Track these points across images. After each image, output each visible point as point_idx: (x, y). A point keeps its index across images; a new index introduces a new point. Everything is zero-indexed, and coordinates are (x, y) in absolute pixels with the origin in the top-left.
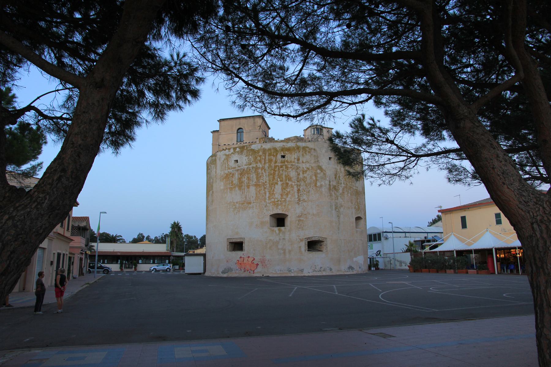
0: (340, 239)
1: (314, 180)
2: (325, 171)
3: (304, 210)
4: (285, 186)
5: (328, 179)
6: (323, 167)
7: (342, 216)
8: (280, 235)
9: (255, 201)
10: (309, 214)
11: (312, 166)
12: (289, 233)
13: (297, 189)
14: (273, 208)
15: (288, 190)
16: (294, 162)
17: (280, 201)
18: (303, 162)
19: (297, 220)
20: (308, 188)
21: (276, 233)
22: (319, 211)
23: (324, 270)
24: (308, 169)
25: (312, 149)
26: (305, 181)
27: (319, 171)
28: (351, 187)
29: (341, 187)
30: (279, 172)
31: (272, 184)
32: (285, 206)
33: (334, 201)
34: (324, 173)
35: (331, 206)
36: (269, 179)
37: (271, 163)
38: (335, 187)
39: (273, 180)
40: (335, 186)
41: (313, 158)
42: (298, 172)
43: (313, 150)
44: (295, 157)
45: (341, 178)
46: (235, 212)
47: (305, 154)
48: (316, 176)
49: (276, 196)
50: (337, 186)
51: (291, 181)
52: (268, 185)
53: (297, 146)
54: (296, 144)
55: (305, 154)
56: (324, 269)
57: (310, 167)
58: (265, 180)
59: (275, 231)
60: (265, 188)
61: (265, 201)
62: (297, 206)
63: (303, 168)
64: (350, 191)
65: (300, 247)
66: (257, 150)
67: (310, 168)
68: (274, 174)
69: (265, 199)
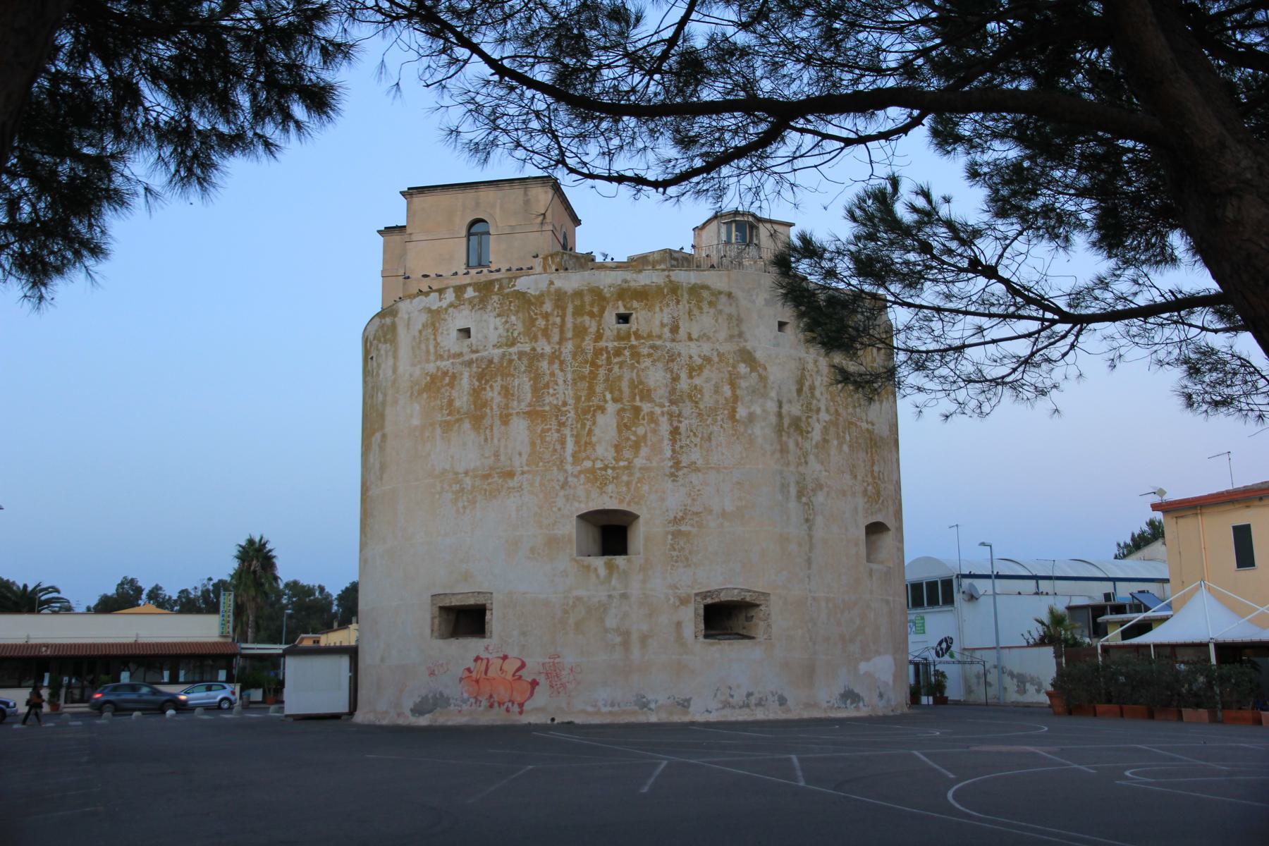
0: (814, 598)
2: (765, 369)
3: (693, 500)
5: (773, 394)
6: (759, 355)
9: (526, 468)
10: (711, 511)
15: (641, 431)
16: (660, 337)
17: (614, 469)
18: (690, 339)
19: (668, 533)
21: (598, 576)
24: (708, 360)
25: (720, 293)
26: (697, 403)
27: (743, 368)
29: (818, 420)
30: (610, 370)
31: (585, 412)
32: (628, 484)
33: (792, 468)
34: (760, 376)
36: (575, 394)
37: (583, 340)
39: (589, 399)
40: (798, 419)
43: (723, 299)
44: (665, 321)
45: (817, 393)
47: (696, 311)
48: (733, 385)
49: (600, 450)
50: (804, 419)
51: (651, 400)
52: (572, 414)
53: (670, 281)
55: (696, 311)
56: (761, 699)
57: (715, 354)
58: (561, 397)
59: (596, 569)
60: (562, 424)
63: (691, 357)
66: (534, 297)
68: (593, 375)
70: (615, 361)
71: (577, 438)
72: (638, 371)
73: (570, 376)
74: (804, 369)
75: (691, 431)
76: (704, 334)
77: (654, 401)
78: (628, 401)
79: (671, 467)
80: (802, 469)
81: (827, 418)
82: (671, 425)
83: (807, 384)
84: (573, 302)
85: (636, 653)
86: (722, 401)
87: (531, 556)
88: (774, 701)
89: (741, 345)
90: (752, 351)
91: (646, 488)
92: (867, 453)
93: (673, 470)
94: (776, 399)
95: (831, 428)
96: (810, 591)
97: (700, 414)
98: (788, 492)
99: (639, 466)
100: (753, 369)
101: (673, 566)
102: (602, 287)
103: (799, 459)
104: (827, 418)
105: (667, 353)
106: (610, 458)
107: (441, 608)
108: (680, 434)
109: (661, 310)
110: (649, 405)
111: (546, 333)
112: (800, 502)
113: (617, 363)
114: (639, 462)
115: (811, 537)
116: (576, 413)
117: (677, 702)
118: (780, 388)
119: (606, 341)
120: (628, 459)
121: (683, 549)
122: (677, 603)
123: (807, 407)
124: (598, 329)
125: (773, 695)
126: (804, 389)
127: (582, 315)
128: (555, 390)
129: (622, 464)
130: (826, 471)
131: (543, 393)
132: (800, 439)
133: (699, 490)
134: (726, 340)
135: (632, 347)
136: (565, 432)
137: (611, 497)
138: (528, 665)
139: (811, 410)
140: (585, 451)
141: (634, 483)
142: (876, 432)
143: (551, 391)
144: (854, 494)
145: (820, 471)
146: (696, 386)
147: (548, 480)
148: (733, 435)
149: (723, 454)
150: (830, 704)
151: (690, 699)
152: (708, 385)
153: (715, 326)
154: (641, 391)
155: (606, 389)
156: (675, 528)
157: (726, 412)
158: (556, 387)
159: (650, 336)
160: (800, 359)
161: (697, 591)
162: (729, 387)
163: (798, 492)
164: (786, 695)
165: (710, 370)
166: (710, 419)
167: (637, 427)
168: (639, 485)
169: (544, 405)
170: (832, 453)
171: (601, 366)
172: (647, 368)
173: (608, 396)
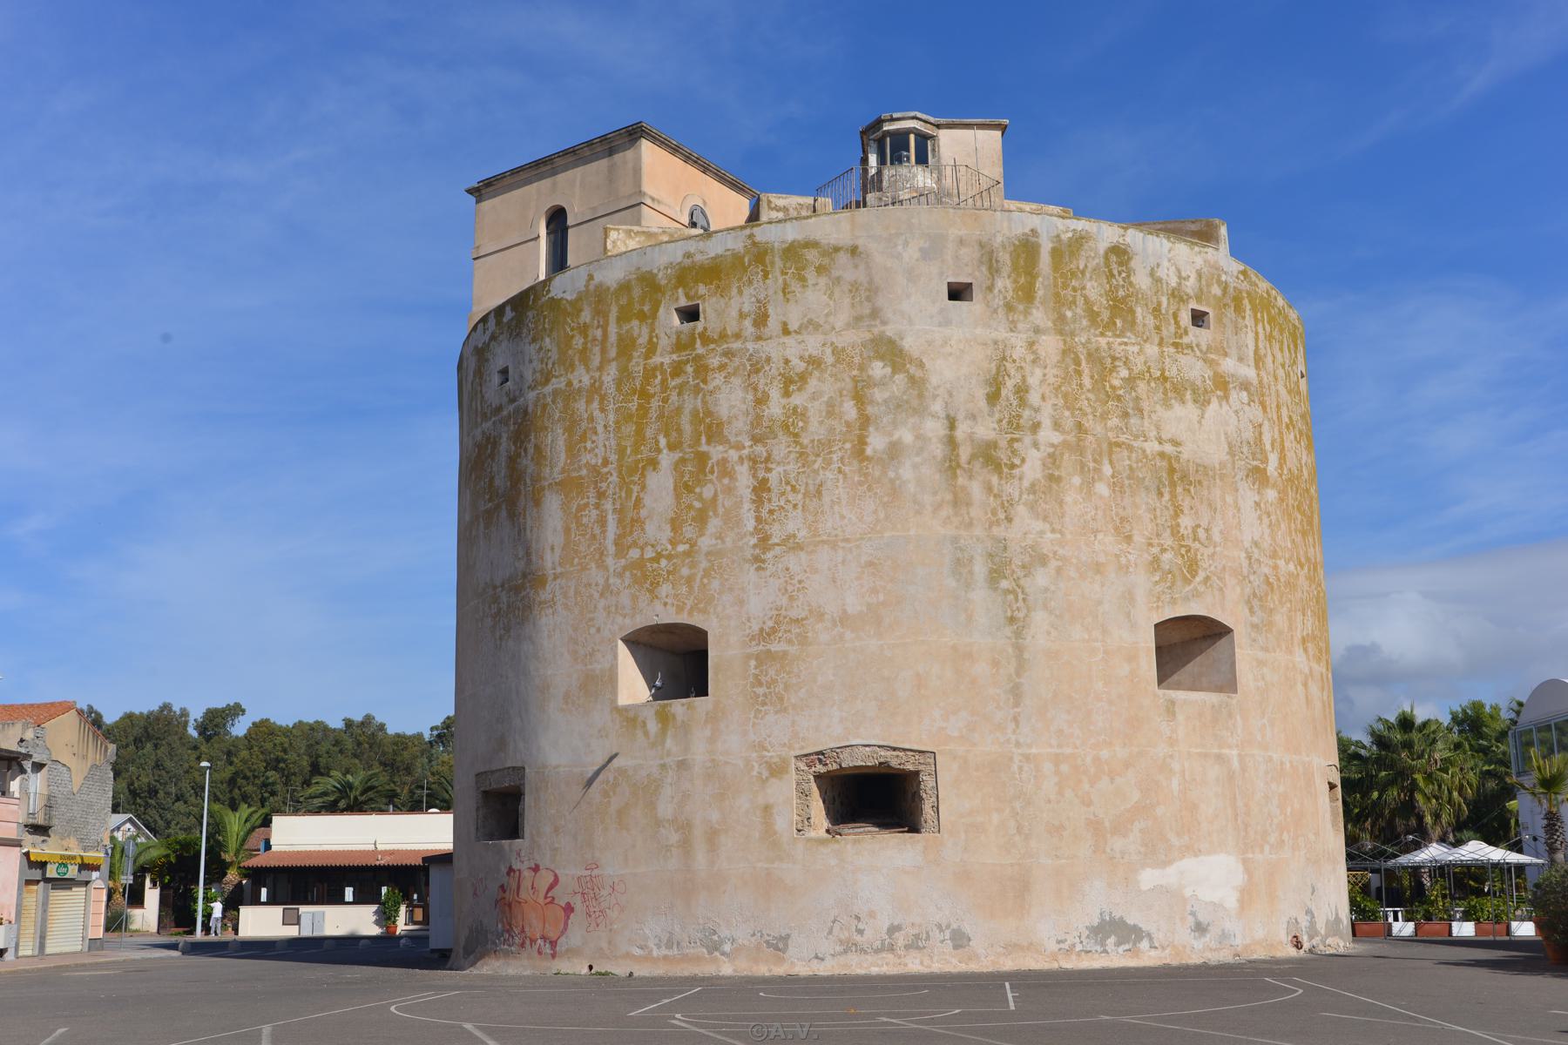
0: (1027, 758)
1: (848, 424)
2: (921, 365)
3: (791, 598)
4: (695, 470)
5: (937, 407)
6: (909, 344)
7: (1039, 618)
8: (663, 743)
9: (559, 570)
10: (821, 616)
11: (840, 342)
12: (708, 733)
13: (751, 482)
14: (634, 598)
15: (708, 492)
16: (737, 336)
17: (669, 557)
18: (786, 331)
19: (749, 657)
20: (816, 472)
21: (646, 734)
22: (881, 597)
23: (914, 945)
24: (815, 362)
25: (837, 249)
26: (796, 435)
27: (878, 369)
28: (1111, 445)
29: (1036, 445)
30: (665, 400)
31: (632, 472)
32: (689, 580)
33: (978, 531)
34: (912, 379)
35: (961, 565)
36: (618, 445)
37: (630, 358)
38: (987, 455)
39: (636, 451)
40: (993, 445)
41: (847, 301)
42: (755, 389)
43: (843, 258)
44: (746, 308)
45: (1034, 398)
46: (498, 634)
47: (795, 286)
48: (860, 399)
49: (651, 530)
50: (1003, 444)
51: (724, 441)
52: (614, 478)
53: (754, 244)
54: (751, 236)
55: (795, 286)
56: (917, 937)
57: (829, 351)
58: (600, 451)
59: (644, 724)
60: (601, 495)
61: (601, 565)
62: (750, 575)
63: (787, 362)
64: (1107, 470)
65: (767, 809)
66: (570, 303)
67: (829, 359)
68: (643, 410)
69: (602, 553)
70: (673, 383)
71: (620, 512)
72: (704, 396)
73: (612, 417)
74: (1004, 359)
75: (788, 483)
76: (810, 322)
77: (728, 442)
78: (690, 446)
79: (755, 546)
80: (997, 531)
81: (1056, 438)
82: (754, 476)
83: (1010, 383)
84: (617, 301)
85: (701, 858)
86: (840, 427)
87: (564, 706)
88: (942, 942)
89: (876, 331)
90: (896, 338)
91: (715, 584)
92: (1160, 494)
93: (757, 551)
94: (943, 415)
95: (1066, 456)
96: (1018, 744)
97: (801, 454)
98: (971, 573)
99: (705, 549)
100: (896, 369)
101: (759, 711)
102: (655, 271)
103: (994, 513)
104: (1056, 438)
105: (749, 360)
106: (664, 541)
107: (486, 793)
108: (769, 490)
109: (740, 292)
110: (720, 448)
111: (585, 360)
112: (996, 589)
113: (675, 388)
114: (705, 543)
115: (1019, 650)
116: (620, 475)
117: (767, 942)
118: (951, 395)
119: (661, 355)
120: (690, 539)
121: (774, 681)
122: (765, 774)
123: (1010, 422)
124: (651, 338)
125: (941, 930)
126: (1004, 392)
127: (628, 320)
128: (593, 442)
129: (681, 548)
130: (1053, 531)
131: (579, 450)
132: (995, 479)
133: (800, 582)
134: (848, 326)
135: (698, 358)
136: (605, 507)
137: (666, 604)
138: (562, 879)
139: (1018, 427)
140: (631, 532)
141: (699, 576)
142: (1185, 456)
143: (589, 445)
144: (1124, 569)
145: (1042, 533)
146: (795, 409)
147: (585, 586)
148: (860, 483)
149: (843, 517)
150: (1065, 946)
151: (788, 936)
152: (816, 404)
153: (828, 305)
154: (710, 427)
155: (659, 431)
156: (761, 647)
157: (848, 446)
158: (594, 438)
159: (723, 336)
160: (996, 343)
161: (799, 753)
162: (852, 403)
163: (991, 571)
164: (967, 929)
165: (819, 380)
166: (820, 460)
167: (702, 487)
168: (705, 581)
169: (580, 468)
170: (1068, 499)
171: (653, 396)
172: (718, 388)
173: (663, 442)
